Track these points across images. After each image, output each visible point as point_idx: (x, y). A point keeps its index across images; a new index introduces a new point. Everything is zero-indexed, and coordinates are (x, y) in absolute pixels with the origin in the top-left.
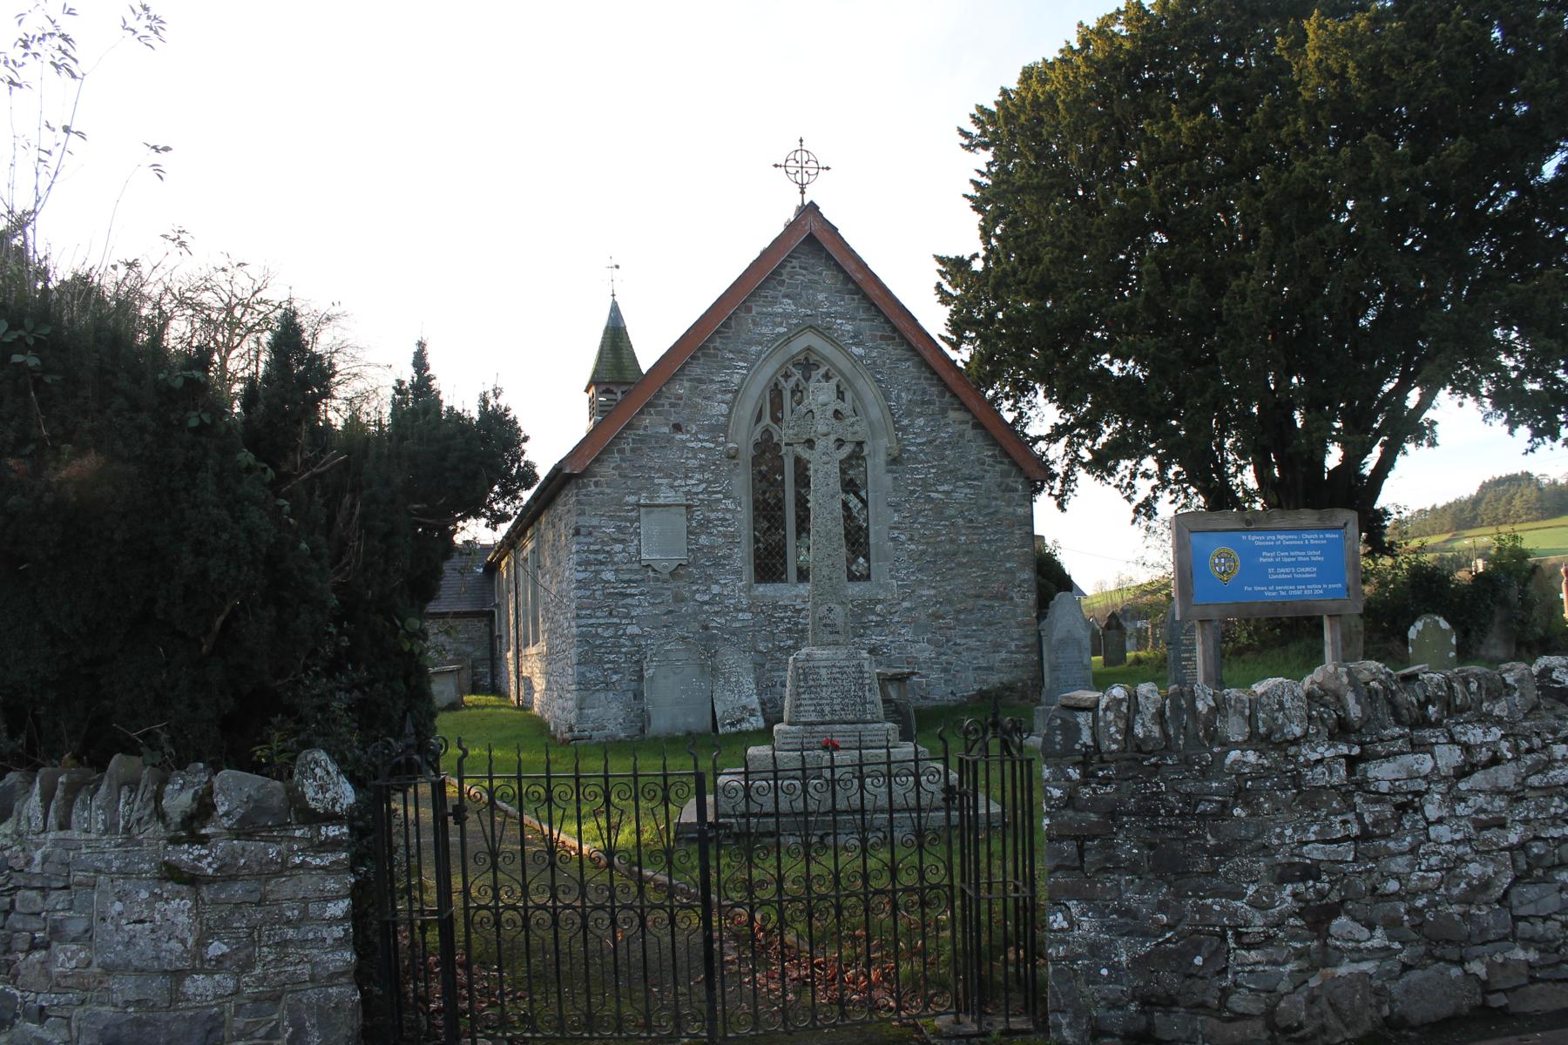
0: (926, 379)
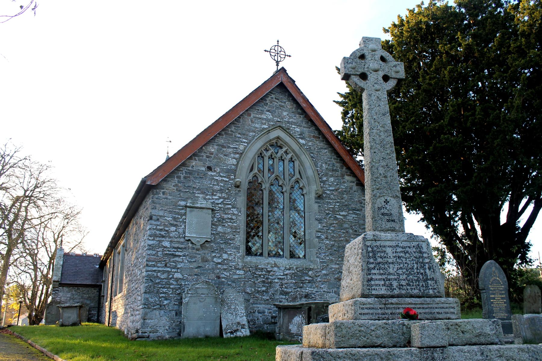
0: (334, 159)
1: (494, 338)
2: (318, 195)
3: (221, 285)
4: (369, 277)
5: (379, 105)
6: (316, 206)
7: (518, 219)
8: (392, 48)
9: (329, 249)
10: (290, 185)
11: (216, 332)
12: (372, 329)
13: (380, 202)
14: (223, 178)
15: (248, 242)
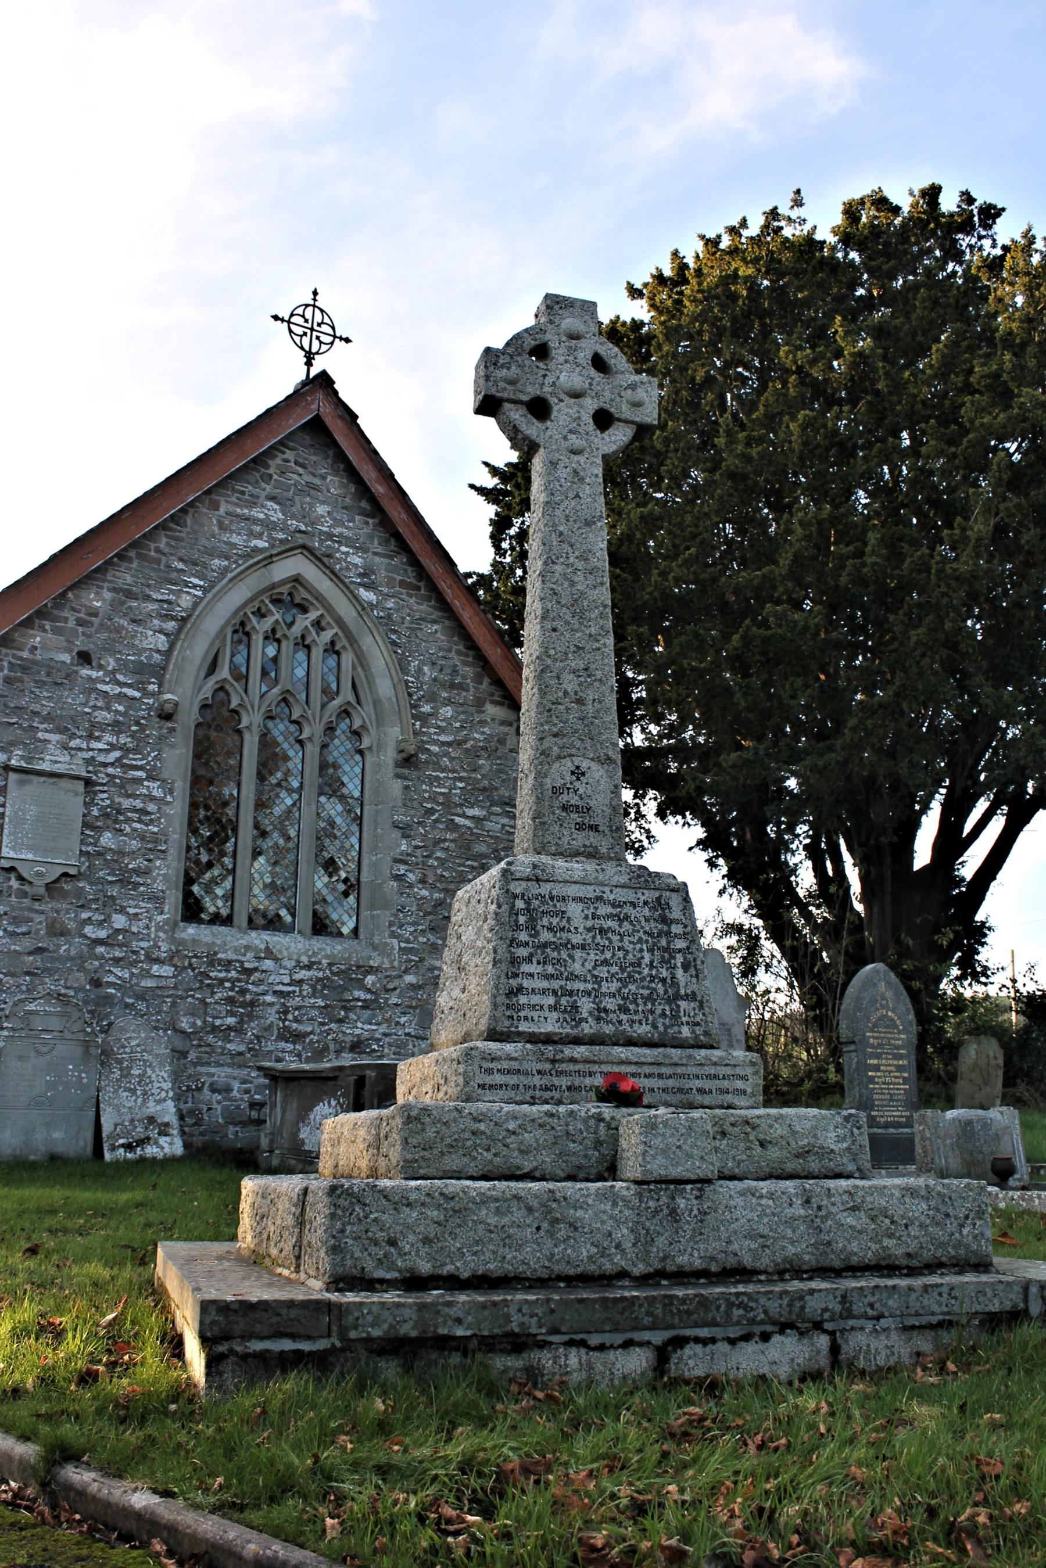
0: (459, 653)
1: (845, 1160)
2: (404, 755)
3: (104, 1005)
4: (514, 982)
5: (577, 496)
6: (397, 786)
7: (961, 855)
8: (650, 345)
9: (426, 914)
10: (325, 720)
11: (82, 1143)
12: (510, 1127)
13: (560, 772)
14: (124, 690)
15: (189, 881)
